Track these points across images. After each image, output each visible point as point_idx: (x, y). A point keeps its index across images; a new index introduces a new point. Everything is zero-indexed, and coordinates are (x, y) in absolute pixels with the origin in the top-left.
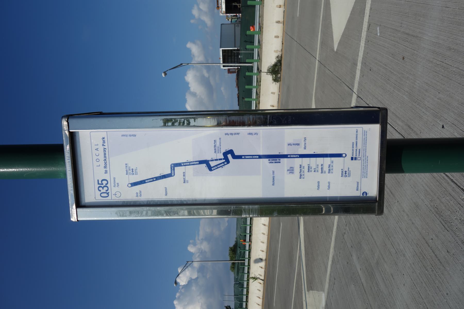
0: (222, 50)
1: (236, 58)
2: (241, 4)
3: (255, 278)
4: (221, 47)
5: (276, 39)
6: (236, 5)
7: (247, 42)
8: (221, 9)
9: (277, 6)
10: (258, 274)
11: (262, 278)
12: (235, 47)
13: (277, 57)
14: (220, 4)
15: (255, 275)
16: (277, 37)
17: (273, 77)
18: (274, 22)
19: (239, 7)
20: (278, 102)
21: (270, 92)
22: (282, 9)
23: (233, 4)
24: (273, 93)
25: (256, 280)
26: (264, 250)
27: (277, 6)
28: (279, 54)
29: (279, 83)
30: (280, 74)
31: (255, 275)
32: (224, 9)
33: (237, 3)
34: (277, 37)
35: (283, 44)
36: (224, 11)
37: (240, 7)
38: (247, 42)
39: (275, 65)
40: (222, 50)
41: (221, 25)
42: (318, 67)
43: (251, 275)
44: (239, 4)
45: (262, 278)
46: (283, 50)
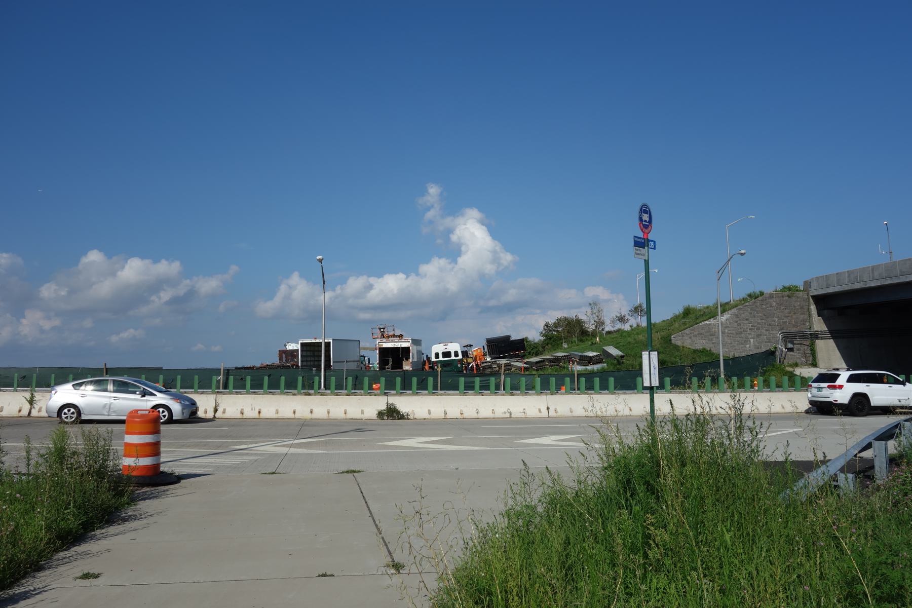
0: (330, 342)
1: (312, 363)
2: (390, 369)
3: (31, 402)
4: (333, 340)
5: (274, 411)
6: (389, 363)
7: (356, 379)
8: (385, 341)
9: (461, 410)
10: (41, 406)
11: (35, 413)
12: (334, 362)
13: (408, 415)
14: (392, 340)
15: (40, 400)
16: (277, 412)
17: (384, 410)
18: (445, 409)
19: (387, 367)
20: (352, 419)
21: (363, 409)
22: (459, 416)
23: (390, 359)
24: (362, 412)
25: (28, 402)
26: (261, 414)
27: (461, 410)
28: (411, 417)
29: (377, 418)
30: (387, 419)
31: (40, 400)
32: (385, 345)
33: (391, 365)
34: (429, 412)
35: (425, 419)
36: (382, 345)
37: (387, 369)
38: (356, 379)
39: (398, 412)
40: (330, 342)
41: (359, 341)
42: (317, 450)
43: (39, 394)
44: (390, 367)
45: (35, 413)
46: (416, 420)
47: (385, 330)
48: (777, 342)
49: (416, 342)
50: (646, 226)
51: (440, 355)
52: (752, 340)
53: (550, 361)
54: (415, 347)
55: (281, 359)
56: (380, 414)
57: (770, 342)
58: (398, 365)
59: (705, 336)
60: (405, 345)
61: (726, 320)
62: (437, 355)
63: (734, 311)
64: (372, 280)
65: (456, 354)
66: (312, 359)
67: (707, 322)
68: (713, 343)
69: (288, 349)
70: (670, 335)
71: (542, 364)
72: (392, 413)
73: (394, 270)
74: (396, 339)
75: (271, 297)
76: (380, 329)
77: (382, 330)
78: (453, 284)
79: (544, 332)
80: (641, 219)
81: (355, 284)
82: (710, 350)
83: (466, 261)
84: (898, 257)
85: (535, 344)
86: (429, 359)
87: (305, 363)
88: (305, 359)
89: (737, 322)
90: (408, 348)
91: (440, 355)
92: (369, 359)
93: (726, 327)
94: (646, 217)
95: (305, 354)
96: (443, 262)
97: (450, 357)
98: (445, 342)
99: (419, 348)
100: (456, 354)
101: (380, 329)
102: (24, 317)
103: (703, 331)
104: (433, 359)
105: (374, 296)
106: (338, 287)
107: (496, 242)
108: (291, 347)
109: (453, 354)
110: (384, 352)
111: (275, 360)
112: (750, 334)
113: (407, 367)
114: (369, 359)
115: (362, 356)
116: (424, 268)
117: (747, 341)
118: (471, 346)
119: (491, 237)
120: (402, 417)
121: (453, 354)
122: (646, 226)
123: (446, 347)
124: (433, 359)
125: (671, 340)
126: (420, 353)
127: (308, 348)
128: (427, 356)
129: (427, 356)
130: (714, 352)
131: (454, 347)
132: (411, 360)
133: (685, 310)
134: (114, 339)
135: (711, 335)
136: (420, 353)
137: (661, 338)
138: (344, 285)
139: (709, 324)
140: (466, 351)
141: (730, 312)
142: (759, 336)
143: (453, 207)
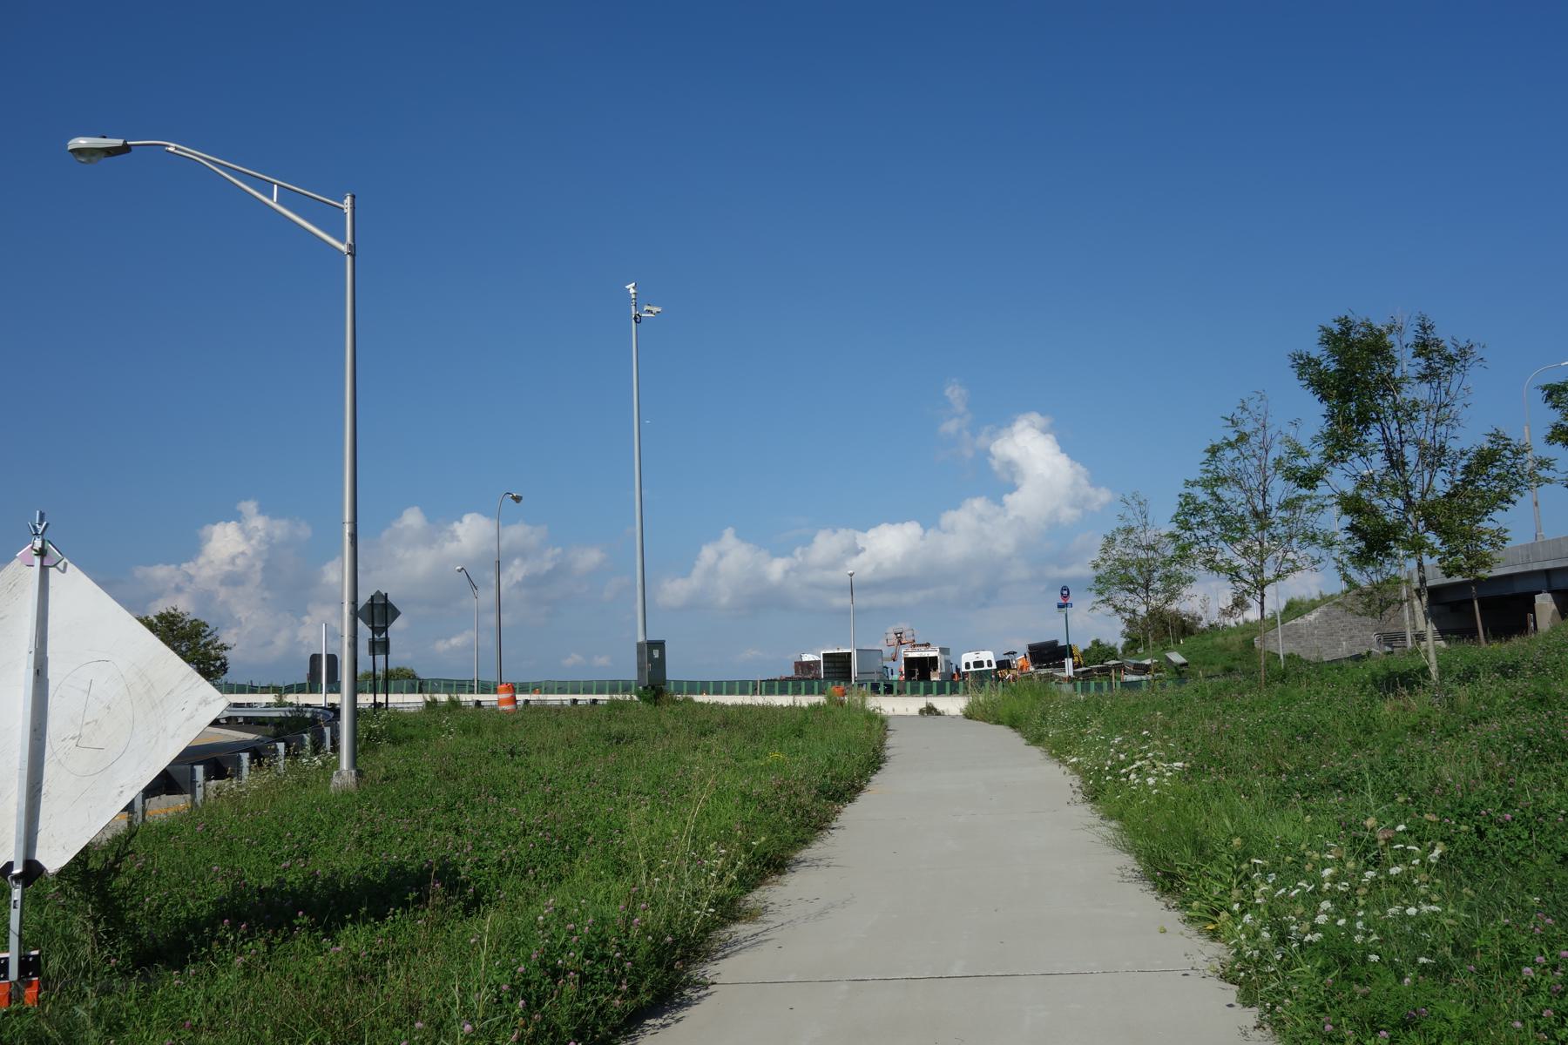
23: (917, 670)
28: (946, 714)
32: (911, 655)
39: (935, 710)
47: (903, 636)
48: (1371, 645)
49: (944, 651)
50: (1065, 597)
51: (972, 665)
52: (1344, 643)
53: (1099, 670)
54: (943, 656)
55: (797, 672)
56: (921, 711)
57: (1364, 645)
58: (925, 676)
59: (1293, 639)
60: (932, 654)
61: (1316, 619)
62: (967, 665)
63: (1323, 608)
64: (860, 536)
65: (990, 663)
66: (834, 671)
67: (1293, 622)
68: (1302, 647)
69: (804, 660)
70: (1252, 639)
71: (1089, 674)
72: (930, 710)
73: (896, 517)
74: (923, 648)
75: (686, 574)
76: (896, 634)
77: (899, 635)
78: (1005, 543)
79: (1127, 630)
80: (1062, 594)
81: (826, 544)
82: (1299, 656)
83: (1026, 502)
84: (1548, 535)
85: (1110, 648)
86: (958, 670)
87: (827, 675)
88: (827, 670)
89: (1327, 621)
90: (936, 658)
91: (972, 665)
92: (892, 670)
93: (1316, 628)
94: (1065, 592)
95: (826, 665)
96: (978, 504)
97: (983, 666)
98: (977, 650)
99: (947, 657)
100: (990, 663)
101: (896, 634)
102: (308, 613)
103: (1289, 633)
104: (963, 669)
105: (860, 566)
106: (798, 551)
107: (1079, 467)
108: (807, 658)
109: (986, 664)
110: (910, 662)
111: (791, 673)
112: (1342, 636)
113: (935, 678)
114: (892, 670)
115: (885, 667)
116: (949, 518)
117: (1339, 644)
118: (1014, 653)
119: (1065, 455)
120: (939, 714)
121: (986, 664)
122: (1065, 597)
123: (978, 655)
124: (963, 669)
125: (1253, 644)
126: (948, 663)
127: (830, 659)
128: (956, 667)
129: (956, 667)
130: (1304, 657)
131: (987, 656)
132: (939, 671)
133: (1287, 603)
134: (442, 646)
135: (1300, 637)
136: (948, 663)
137: (1243, 641)
138: (807, 549)
139: (1297, 624)
140: (1008, 660)
141: (1319, 609)
142: (1352, 637)
143: (1000, 418)
